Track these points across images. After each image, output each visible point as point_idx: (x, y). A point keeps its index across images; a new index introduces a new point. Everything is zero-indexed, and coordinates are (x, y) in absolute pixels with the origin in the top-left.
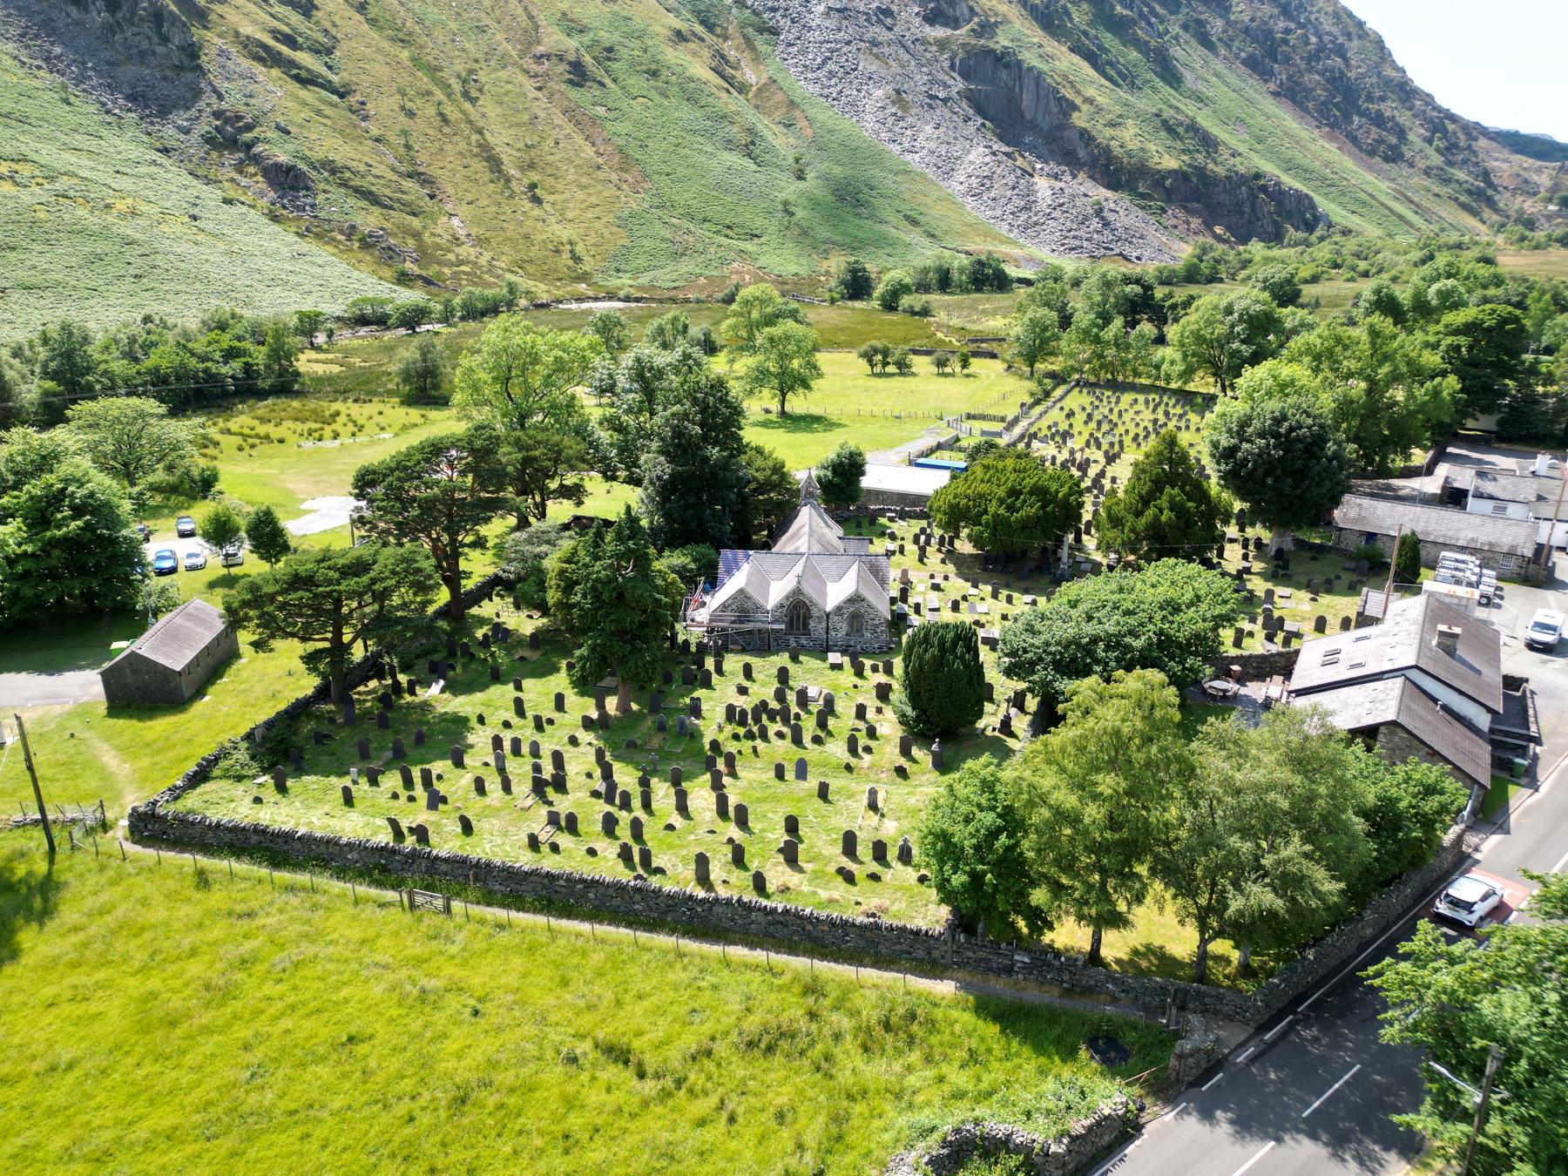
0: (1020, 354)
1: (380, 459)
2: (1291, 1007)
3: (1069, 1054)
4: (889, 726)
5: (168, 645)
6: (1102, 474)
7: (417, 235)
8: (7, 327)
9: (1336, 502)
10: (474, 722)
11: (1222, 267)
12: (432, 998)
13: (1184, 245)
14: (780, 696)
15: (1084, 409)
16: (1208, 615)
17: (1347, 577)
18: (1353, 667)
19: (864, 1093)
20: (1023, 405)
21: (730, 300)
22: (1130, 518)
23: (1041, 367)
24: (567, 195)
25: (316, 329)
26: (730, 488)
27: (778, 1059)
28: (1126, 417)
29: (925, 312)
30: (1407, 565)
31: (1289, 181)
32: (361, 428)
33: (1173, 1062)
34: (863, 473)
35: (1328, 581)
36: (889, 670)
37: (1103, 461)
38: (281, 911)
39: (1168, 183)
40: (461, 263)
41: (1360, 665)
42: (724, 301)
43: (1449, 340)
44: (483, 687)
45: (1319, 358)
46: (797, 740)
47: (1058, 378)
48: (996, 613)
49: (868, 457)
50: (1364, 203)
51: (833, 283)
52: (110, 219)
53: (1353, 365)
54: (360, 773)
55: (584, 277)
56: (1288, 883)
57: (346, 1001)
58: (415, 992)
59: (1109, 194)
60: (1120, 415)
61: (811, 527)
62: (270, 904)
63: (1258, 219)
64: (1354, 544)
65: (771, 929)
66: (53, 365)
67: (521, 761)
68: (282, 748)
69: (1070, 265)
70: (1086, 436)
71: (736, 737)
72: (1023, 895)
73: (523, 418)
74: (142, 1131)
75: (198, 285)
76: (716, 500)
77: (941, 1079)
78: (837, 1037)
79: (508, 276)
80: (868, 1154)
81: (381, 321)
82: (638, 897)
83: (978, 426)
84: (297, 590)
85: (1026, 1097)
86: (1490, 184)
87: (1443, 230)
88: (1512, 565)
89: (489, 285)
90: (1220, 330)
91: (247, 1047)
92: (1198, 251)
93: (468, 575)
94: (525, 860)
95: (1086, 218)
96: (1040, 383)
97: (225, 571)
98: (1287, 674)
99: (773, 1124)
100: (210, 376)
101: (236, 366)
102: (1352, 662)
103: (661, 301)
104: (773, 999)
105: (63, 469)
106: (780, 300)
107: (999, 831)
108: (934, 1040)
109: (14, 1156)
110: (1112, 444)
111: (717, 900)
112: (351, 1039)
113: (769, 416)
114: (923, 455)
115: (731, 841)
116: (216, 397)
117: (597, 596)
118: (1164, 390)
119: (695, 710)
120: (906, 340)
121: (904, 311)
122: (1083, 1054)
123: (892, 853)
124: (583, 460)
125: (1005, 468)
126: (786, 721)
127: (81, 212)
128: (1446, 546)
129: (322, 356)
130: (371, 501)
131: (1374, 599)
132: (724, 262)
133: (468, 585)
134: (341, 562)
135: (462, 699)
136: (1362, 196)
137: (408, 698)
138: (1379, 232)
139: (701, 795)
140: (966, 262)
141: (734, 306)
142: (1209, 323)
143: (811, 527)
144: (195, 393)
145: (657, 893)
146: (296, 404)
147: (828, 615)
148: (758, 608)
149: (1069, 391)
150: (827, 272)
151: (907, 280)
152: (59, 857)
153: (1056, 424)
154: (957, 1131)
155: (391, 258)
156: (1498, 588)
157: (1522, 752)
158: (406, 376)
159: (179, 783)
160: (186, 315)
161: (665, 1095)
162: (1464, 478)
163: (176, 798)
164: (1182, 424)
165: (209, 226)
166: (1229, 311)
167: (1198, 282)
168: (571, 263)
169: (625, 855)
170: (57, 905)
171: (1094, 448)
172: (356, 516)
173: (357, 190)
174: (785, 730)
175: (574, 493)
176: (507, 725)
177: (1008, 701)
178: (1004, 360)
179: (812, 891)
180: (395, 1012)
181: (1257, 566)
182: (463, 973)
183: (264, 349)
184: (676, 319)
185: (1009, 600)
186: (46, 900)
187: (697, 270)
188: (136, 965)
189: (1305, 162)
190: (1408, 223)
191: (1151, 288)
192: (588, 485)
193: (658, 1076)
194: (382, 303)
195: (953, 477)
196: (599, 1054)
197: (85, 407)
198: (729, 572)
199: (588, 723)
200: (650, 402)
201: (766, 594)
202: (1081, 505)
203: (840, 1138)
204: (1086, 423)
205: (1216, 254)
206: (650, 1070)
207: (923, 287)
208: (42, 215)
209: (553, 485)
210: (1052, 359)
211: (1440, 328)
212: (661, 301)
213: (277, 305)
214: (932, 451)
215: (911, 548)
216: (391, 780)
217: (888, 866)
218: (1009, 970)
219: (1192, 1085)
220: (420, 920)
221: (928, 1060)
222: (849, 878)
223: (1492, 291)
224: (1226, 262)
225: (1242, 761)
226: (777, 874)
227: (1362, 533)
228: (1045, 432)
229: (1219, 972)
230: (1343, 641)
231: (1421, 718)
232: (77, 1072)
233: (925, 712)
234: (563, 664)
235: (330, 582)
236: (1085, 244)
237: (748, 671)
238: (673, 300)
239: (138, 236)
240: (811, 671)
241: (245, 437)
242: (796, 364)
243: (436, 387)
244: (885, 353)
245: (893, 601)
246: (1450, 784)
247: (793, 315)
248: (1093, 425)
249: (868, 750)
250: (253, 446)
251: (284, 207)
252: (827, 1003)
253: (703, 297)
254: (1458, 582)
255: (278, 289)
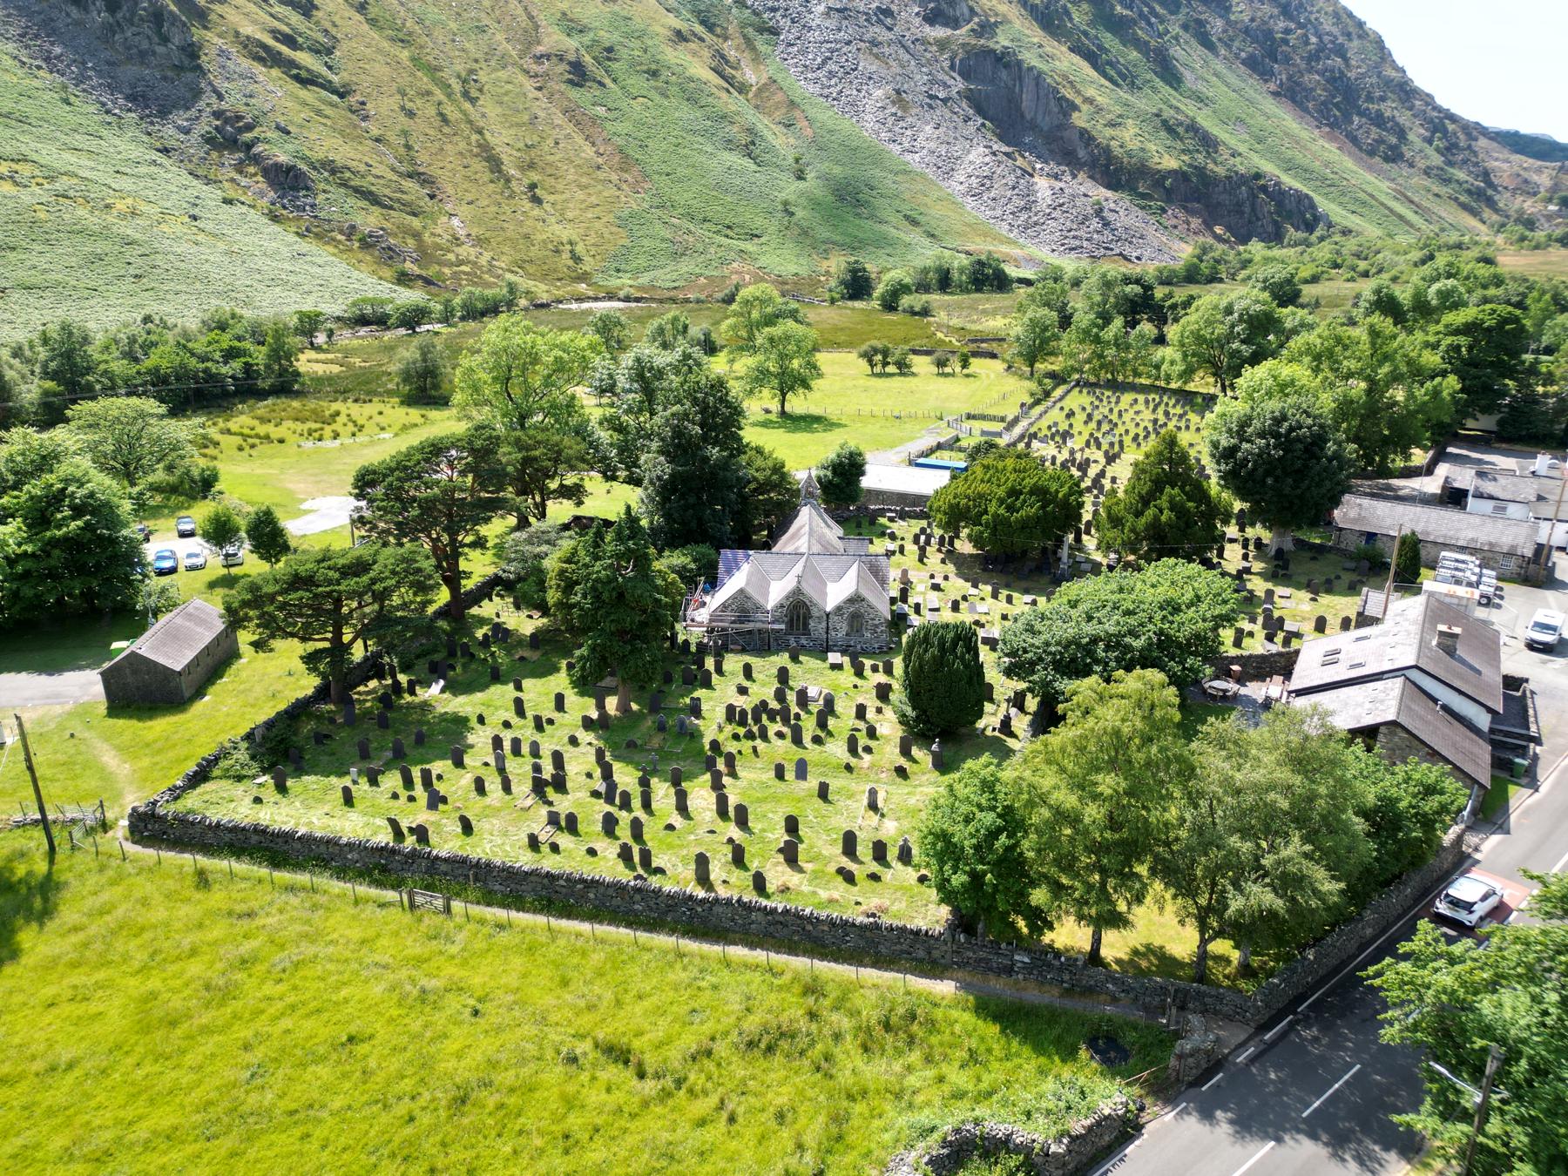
0: (1020, 354)
1: (380, 459)
2: (1291, 1007)
3: (1069, 1054)
4: (889, 726)
5: (168, 645)
6: (1102, 474)
7: (417, 235)
8: (7, 327)
9: (1336, 502)
10: (474, 722)
11: (1222, 267)
12: (432, 998)
13: (1184, 245)
14: (780, 696)
15: (1084, 409)
16: (1208, 615)
17: (1347, 577)
18: (1353, 667)
19: (864, 1093)
20: (1023, 405)
21: (730, 300)
22: (1130, 518)
23: (1041, 367)
24: (567, 195)
25: (316, 329)
26: (730, 488)
27: (778, 1059)
28: (1126, 417)
29: (925, 312)
30: (1407, 565)
31: (1289, 181)
32: (361, 428)
33: (1173, 1062)
34: (863, 473)
35: (1328, 581)
36: (889, 670)
37: (1103, 461)
38: (281, 911)
39: (1168, 183)
40: (461, 263)
41: (1360, 665)
42: (724, 301)
43: (1449, 340)
44: (483, 687)
45: (1319, 358)
46: (797, 740)
47: (1058, 378)
48: (996, 613)
49: (868, 457)
50: (1364, 203)
51: (833, 283)
52: (110, 219)
53: (1353, 365)
54: (360, 773)
55: (584, 277)
56: (1288, 883)
57: (346, 1001)
58: (415, 992)
59: (1109, 194)
60: (1120, 415)
61: (811, 527)
62: (270, 904)
63: (1258, 219)
64: (1354, 544)
65: (771, 929)
66: (53, 365)
67: (521, 761)
68: (282, 748)
69: (1070, 265)
70: (1086, 436)
71: (736, 737)
72: (1023, 895)
73: (523, 418)
74: (142, 1131)
75: (198, 285)
76: (716, 500)
77: (941, 1079)
78: (837, 1037)
79: (508, 276)
80: (868, 1154)
81: (381, 321)
82: (638, 897)
83: (978, 426)
84: (297, 590)
85: (1026, 1097)
86: (1490, 184)
87: (1443, 230)
88: (1512, 565)
89: (489, 285)
90: (1220, 330)
91: (247, 1047)
92: (1198, 251)
93: (468, 575)
94: (525, 860)
95: (1086, 218)
96: (1040, 383)
97: (225, 571)
98: (1287, 674)
99: (773, 1124)
100: (210, 376)
101: (236, 366)
102: (1352, 662)
103: (661, 301)
104: (773, 999)
105: (63, 469)
106: (780, 300)
107: (999, 831)
108: (934, 1040)
109: (14, 1156)
110: (1112, 444)
111: (717, 900)
112: (351, 1039)
113: (769, 416)
114: (923, 455)
115: (731, 841)
116: (216, 397)
117: (597, 596)
118: (1164, 390)
119: (695, 710)
120: (906, 340)
121: (904, 311)
122: (1083, 1054)
123: (892, 853)
124: (583, 460)
125: (1005, 468)
126: (786, 721)
127: (81, 212)
128: (1446, 546)
129: (322, 356)
130: (371, 501)
131: (1374, 599)
132: (724, 262)
133: (468, 585)
134: (341, 562)
135: (462, 699)
136: (1362, 196)
137: (408, 698)
138: (1379, 232)
139: (701, 795)
140: (966, 262)
141: (734, 306)
142: (1209, 323)
143: (811, 527)
144: (195, 393)
145: (657, 893)
146: (296, 404)
147: (828, 615)
148: (758, 608)
149: (1069, 391)
150: (827, 272)
151: (907, 280)
152: (59, 857)
153: (1056, 424)
154: (957, 1131)
155: (391, 258)
156: (1498, 588)
157: (1522, 752)
158: (406, 376)
159: (179, 783)
160: (186, 315)
161: (665, 1095)
162: (1464, 478)
163: (176, 798)
164: (1182, 424)
165: (209, 226)
166: (1229, 311)
167: (1198, 282)
168: (571, 263)
169: (625, 855)
170: (57, 905)
171: (1094, 448)
172: (356, 516)
173: (357, 190)
174: (785, 730)
175: (574, 493)
176: (507, 725)
177: (1008, 701)
178: (1004, 360)
179: (812, 891)
180: (395, 1012)
181: (1257, 566)
182: (463, 973)
183: (264, 349)
184: (676, 319)
185: (1009, 600)
186: (46, 900)
187: (697, 270)
188: (136, 965)
189: (1305, 162)
190: (1408, 223)
191: (1151, 288)
192: (588, 485)
193: (658, 1076)
194: (382, 303)
195: (953, 477)
196: (599, 1054)
197: (85, 407)
198: (729, 572)
199: (588, 723)
200: (650, 402)
201: (766, 594)
202: (1081, 505)
203: (840, 1138)
204: (1086, 423)
205: (1216, 254)
206: (650, 1070)
207: (923, 287)
208: (42, 215)
209: (553, 485)
210: (1052, 359)
211: (1440, 328)
212: (661, 301)
213: (277, 305)
214: (932, 451)
215: (911, 548)
216: (391, 780)
217: (888, 866)
218: (1009, 970)
219: (1192, 1085)
220: (420, 920)
221: (928, 1060)
222: (849, 878)
223: (1492, 291)
224: (1226, 262)
225: (1242, 761)
226: (777, 874)
227: (1362, 533)
228: (1045, 432)
229: (1219, 972)
230: (1343, 641)
231: (1421, 718)
232: (77, 1072)
233: (925, 712)
234: (563, 664)
235: (330, 582)
236: (1085, 244)
237: (748, 671)
238: (673, 300)
239: (138, 236)
240: (811, 671)
241: (245, 437)
242: (796, 364)
243: (436, 387)
244: (885, 353)
245: (893, 601)
246: (1450, 784)
247: (793, 315)
248: (1093, 425)
249: (868, 750)
250: (253, 446)
251: (284, 207)
252: (827, 1003)
253: (703, 297)
254: (1458, 582)
255: (278, 289)
